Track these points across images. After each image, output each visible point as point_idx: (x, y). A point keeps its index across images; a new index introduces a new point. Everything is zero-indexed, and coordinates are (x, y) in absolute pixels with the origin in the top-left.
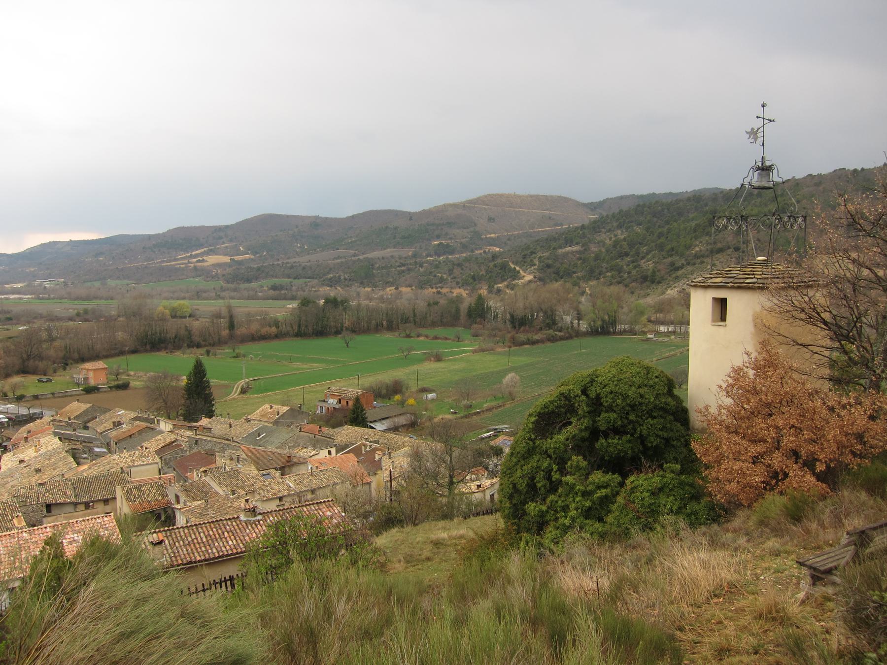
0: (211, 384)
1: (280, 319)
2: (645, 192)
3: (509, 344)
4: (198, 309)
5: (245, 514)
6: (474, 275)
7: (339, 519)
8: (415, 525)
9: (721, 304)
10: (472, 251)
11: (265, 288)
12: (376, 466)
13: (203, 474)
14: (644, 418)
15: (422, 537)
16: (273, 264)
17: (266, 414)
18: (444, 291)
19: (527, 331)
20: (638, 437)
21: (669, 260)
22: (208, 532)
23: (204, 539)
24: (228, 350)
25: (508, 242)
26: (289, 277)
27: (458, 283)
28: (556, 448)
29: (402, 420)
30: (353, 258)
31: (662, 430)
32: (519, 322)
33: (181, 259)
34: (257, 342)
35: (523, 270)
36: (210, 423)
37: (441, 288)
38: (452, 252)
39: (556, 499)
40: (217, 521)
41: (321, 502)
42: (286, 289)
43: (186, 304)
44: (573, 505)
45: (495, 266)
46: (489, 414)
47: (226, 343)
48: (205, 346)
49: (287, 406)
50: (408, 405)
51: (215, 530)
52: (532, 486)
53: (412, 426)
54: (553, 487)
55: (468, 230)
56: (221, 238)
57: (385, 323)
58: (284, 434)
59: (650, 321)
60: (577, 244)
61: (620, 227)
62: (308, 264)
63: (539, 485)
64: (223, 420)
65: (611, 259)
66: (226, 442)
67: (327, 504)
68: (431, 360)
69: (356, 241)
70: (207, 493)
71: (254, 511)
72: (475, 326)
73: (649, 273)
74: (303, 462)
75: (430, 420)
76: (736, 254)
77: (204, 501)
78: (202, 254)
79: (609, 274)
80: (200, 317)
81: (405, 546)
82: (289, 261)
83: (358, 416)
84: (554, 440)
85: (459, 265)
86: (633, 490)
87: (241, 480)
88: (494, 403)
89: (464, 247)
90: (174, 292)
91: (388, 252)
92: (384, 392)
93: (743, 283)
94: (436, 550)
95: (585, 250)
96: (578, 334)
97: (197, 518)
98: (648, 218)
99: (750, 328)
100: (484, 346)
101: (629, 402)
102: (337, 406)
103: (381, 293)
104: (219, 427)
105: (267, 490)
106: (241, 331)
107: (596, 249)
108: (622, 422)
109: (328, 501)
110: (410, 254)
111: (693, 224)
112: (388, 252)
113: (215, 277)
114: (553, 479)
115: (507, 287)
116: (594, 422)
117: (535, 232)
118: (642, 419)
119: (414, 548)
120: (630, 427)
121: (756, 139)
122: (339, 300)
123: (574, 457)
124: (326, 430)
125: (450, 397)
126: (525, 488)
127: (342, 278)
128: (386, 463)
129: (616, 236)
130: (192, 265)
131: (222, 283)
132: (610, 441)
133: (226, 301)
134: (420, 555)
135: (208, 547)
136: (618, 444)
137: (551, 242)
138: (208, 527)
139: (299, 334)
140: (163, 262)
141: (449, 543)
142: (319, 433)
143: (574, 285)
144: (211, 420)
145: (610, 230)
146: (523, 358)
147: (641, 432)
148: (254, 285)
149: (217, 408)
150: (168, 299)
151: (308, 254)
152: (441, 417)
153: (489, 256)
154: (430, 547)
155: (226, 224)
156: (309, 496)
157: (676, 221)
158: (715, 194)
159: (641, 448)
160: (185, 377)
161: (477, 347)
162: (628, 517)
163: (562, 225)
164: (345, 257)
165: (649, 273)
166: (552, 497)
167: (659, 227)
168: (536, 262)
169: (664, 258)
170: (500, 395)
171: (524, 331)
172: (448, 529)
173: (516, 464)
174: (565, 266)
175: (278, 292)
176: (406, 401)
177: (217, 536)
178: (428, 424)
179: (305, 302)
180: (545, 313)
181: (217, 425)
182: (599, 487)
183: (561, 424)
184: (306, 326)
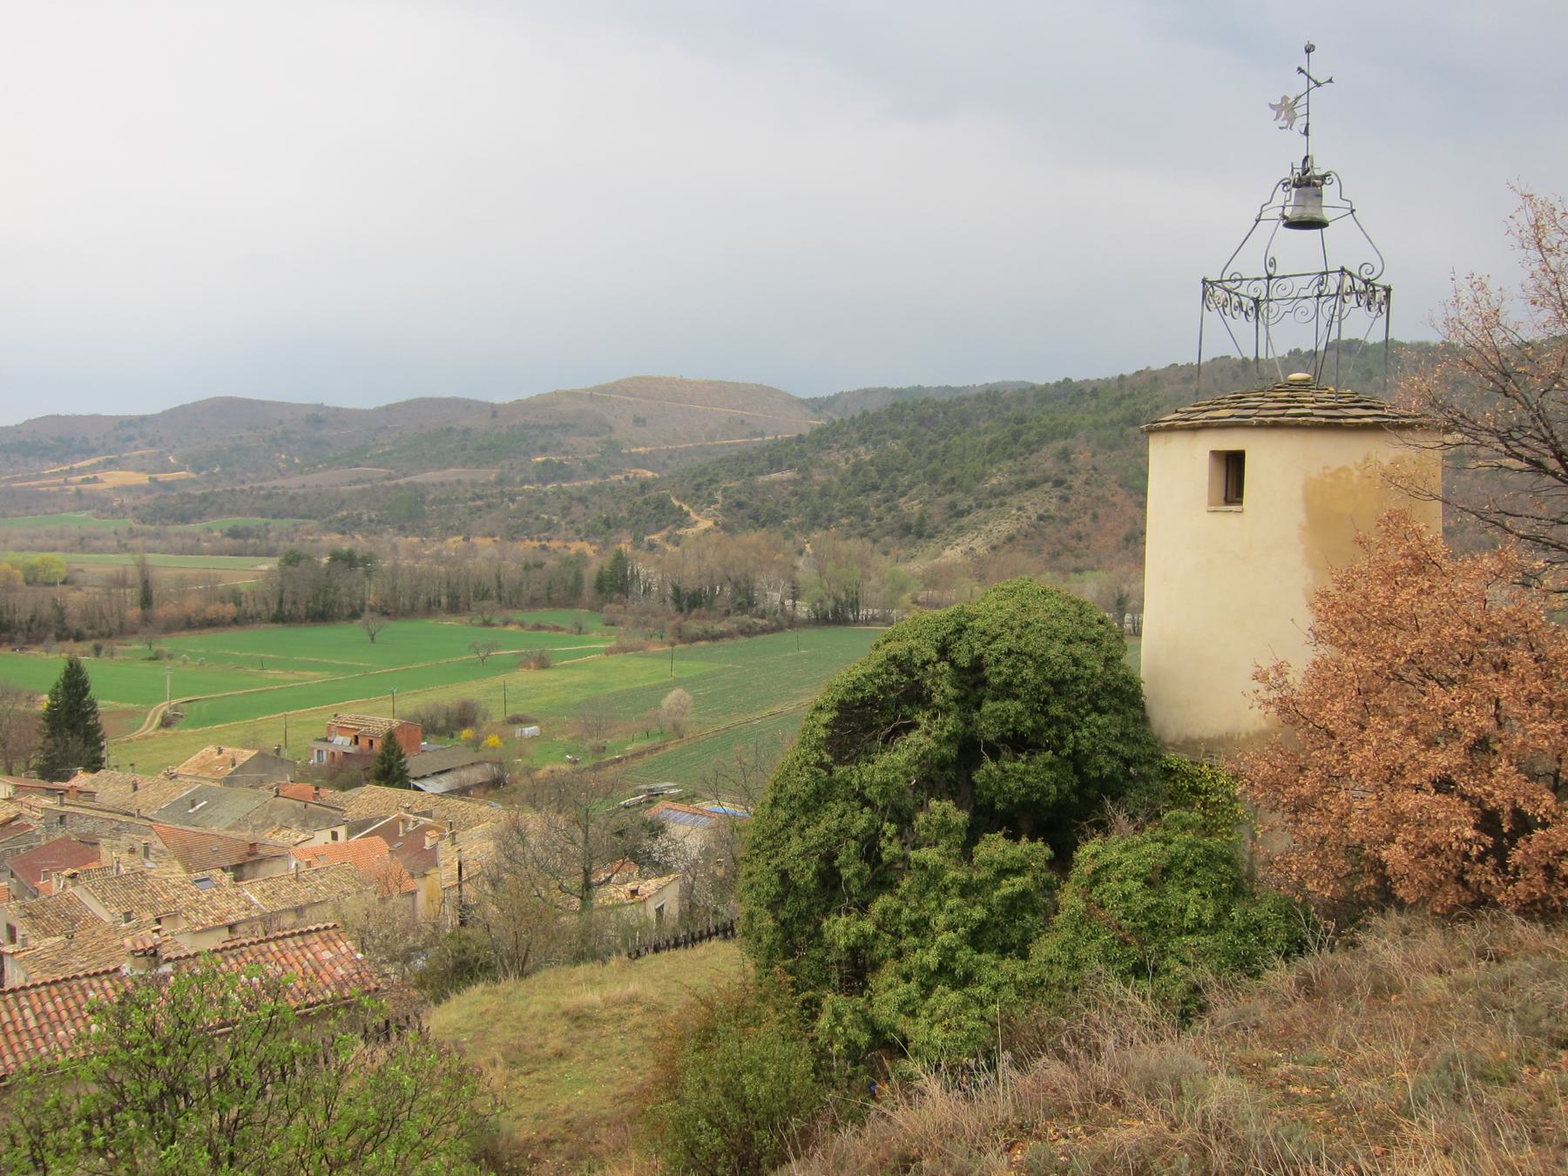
0: (100, 708)
1: (244, 589)
2: (905, 383)
3: (672, 639)
4: (81, 571)
5: (134, 963)
6: (608, 518)
7: (350, 966)
8: (523, 975)
9: (1233, 465)
10: (605, 476)
11: (217, 534)
12: (430, 859)
13: (69, 882)
14: (1082, 711)
15: (543, 1003)
16: (233, 490)
17: (210, 764)
18: (554, 545)
19: (704, 617)
20: (1068, 757)
21: (947, 498)
22: (43, 1005)
23: (32, 1023)
24: (137, 646)
25: (669, 462)
26: (263, 514)
27: (578, 532)
28: (886, 784)
29: (476, 775)
30: (387, 483)
31: (1118, 740)
32: (689, 601)
33: (50, 475)
34: (196, 632)
35: (695, 511)
36: (92, 782)
37: (549, 540)
38: (568, 478)
39: (896, 904)
40: (66, 979)
41: (309, 932)
42: (258, 537)
43: (60, 562)
44: (941, 919)
45: (646, 503)
46: (638, 763)
47: (135, 633)
48: (92, 637)
49: (253, 749)
50: (486, 747)
51: (59, 1000)
52: (829, 879)
53: (495, 785)
54: (882, 881)
55: (597, 439)
56: (131, 439)
57: (444, 600)
58: (243, 802)
59: (915, 602)
60: (790, 467)
61: (863, 440)
62: (301, 492)
63: (846, 873)
64: (119, 775)
65: (849, 494)
66: (125, 819)
67: (324, 934)
68: (530, 667)
69: (390, 453)
70: (74, 920)
71: (155, 954)
72: (608, 606)
73: (914, 521)
74: (279, 856)
75: (529, 775)
76: (1058, 492)
77: (63, 937)
78: (93, 468)
79: (844, 521)
80: (85, 584)
81: (505, 1027)
82: (264, 484)
83: (391, 767)
84: (880, 764)
85: (581, 500)
86: (1096, 879)
87: (150, 891)
88: (646, 744)
89: (591, 468)
90: (33, 537)
91: (451, 474)
92: (441, 723)
93: (1283, 415)
94: (577, 1034)
95: (804, 478)
96: (793, 623)
97: (47, 971)
98: (912, 426)
99: (1298, 515)
100: (626, 642)
101: (1049, 675)
102: (351, 750)
103: (438, 546)
104: (112, 790)
105: (205, 911)
106: (165, 610)
107: (823, 478)
108: (1035, 722)
109: (326, 928)
110: (492, 477)
111: (987, 439)
112: (451, 474)
113: (118, 512)
114: (885, 857)
115: (667, 539)
116: (968, 723)
117: (716, 446)
118: (1078, 713)
119: (525, 1029)
120: (1052, 732)
121: (1291, 120)
122: (358, 555)
123: (933, 803)
124: (329, 794)
125: (564, 732)
126: (812, 881)
127: (365, 517)
128: (448, 856)
129: (856, 456)
130: (73, 488)
131: (130, 522)
132: (1007, 766)
133: (137, 556)
134: (540, 1046)
135: (40, 1041)
136: (1026, 772)
137: (745, 463)
138: (45, 995)
139: (280, 618)
140: (15, 480)
141: (606, 1014)
142: (314, 798)
143: (787, 536)
144: (95, 776)
145: (846, 446)
146: (695, 663)
147: (1077, 742)
148: (195, 527)
149: (111, 751)
150: (23, 550)
151: (302, 473)
152: (549, 767)
153: (636, 484)
154: (563, 1026)
155: (142, 413)
156: (288, 920)
157: (958, 433)
158: (1023, 391)
159: (1076, 780)
160: (46, 697)
161: (614, 643)
162: (1095, 943)
163: (762, 434)
164: (370, 481)
165: (914, 521)
166: (883, 901)
167: (931, 442)
168: (718, 496)
169: (939, 495)
170: (657, 730)
171: (698, 617)
172: (600, 983)
173: (787, 825)
174: (768, 505)
175: (241, 541)
176: (482, 739)
177: (64, 1014)
178: (524, 781)
179: (293, 559)
180: (736, 584)
181: (107, 786)
182: (1003, 872)
183: (888, 730)
184: (294, 603)
